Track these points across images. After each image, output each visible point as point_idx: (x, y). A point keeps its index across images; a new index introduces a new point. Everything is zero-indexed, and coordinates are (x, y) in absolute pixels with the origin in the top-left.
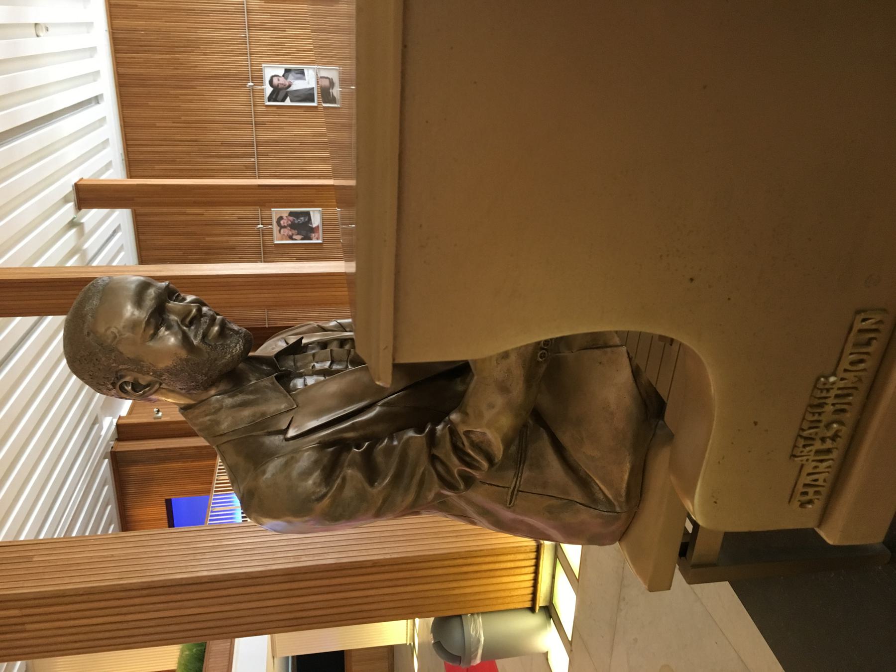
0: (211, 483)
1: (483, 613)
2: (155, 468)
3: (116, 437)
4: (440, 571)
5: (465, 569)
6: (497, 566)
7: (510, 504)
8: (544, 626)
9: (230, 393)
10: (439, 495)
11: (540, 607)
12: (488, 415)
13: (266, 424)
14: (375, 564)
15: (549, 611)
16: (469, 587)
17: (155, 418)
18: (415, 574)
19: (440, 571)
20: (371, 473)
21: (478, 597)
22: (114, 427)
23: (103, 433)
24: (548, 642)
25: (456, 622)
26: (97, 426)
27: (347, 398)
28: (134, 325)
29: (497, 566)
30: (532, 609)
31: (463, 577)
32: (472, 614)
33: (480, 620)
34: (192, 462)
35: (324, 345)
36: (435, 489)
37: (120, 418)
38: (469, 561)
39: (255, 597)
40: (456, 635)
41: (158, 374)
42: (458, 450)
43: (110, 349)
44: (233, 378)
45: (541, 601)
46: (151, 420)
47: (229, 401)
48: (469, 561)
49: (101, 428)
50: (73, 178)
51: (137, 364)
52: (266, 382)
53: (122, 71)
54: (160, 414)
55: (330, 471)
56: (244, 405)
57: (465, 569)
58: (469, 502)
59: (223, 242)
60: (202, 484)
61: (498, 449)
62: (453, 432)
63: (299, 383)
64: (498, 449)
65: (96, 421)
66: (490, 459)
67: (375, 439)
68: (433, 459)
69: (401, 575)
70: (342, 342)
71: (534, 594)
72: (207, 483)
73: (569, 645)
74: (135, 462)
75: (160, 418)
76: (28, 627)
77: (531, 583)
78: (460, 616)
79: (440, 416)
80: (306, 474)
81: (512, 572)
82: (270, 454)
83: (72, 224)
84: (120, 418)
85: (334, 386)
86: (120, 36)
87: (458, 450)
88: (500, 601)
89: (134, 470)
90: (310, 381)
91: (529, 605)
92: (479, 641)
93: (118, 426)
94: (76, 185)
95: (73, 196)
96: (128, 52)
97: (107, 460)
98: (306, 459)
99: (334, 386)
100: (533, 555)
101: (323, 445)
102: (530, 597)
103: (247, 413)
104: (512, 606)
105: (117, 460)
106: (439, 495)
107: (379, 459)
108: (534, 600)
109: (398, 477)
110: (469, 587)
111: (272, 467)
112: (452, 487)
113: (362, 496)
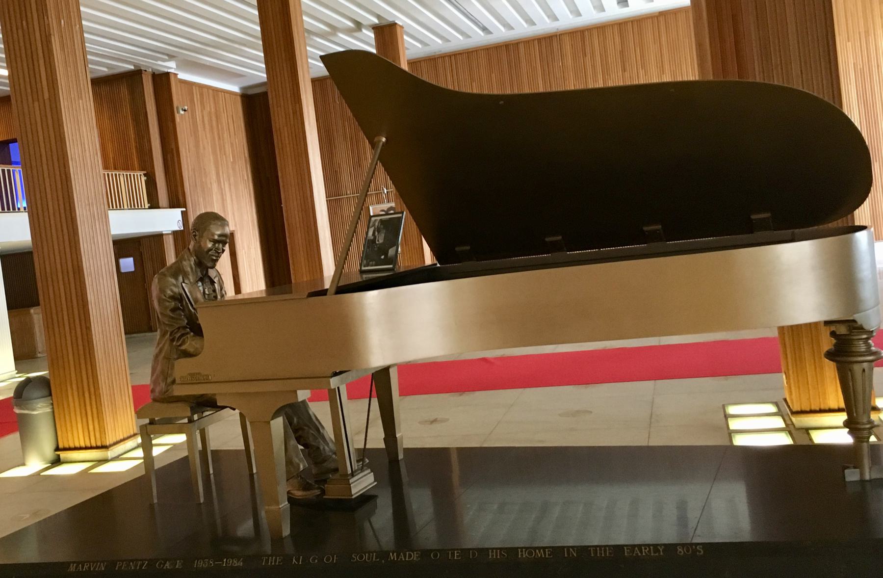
0: (115, 169)
1: (53, 412)
2: (127, 109)
3: (156, 73)
4: (84, 377)
5: (87, 395)
6: (90, 418)
7: (165, 358)
8: (44, 459)
9: (195, 264)
10: (167, 331)
11: (59, 456)
12: (193, 343)
13: (185, 275)
14: (88, 328)
15: (57, 462)
16: (73, 400)
17: (177, 108)
18: (82, 357)
19: (84, 377)
20: (173, 310)
21: (66, 406)
22: (166, 70)
23: (160, 63)
24: (34, 465)
25: (46, 392)
26: (166, 57)
27: (196, 301)
28: (213, 235)
29: (90, 418)
30: (57, 449)
31: (81, 393)
32: (52, 404)
33: (49, 410)
34: (136, 147)
35: (214, 291)
36: (169, 330)
37: (176, 75)
38: (93, 397)
39: (62, 248)
40: (37, 393)
41: (199, 242)
42: (183, 335)
43: (205, 229)
44: (200, 264)
45: (63, 455)
46: (176, 103)
47: (192, 263)
48: (93, 397)
49: (164, 60)
50: (401, 19)
51: (201, 237)
52: (199, 274)
53: (521, 47)
54: (182, 112)
55: (173, 298)
56: (191, 268)
57: (87, 395)
58: (164, 345)
59: (365, 153)
60: (114, 159)
61: (183, 347)
62: (187, 333)
63: (200, 284)
64: (183, 347)
65: (171, 57)
66: (180, 345)
67: (183, 311)
68: (179, 328)
69: (81, 347)
70: (216, 297)
71: (70, 449)
72: (114, 165)
73: (38, 474)
74: (132, 92)
75: (178, 112)
76: (36, 104)
77: (77, 445)
78: (51, 395)
79: (192, 330)
80: (172, 291)
81: (86, 430)
82: (177, 279)
83: (359, 25)
84: (176, 75)
85: (199, 296)
86: (555, 44)
87: (183, 335)
88: (63, 423)
89: (124, 91)
90: (201, 288)
91: (61, 446)
92: (34, 410)
93: (168, 73)
94: (396, 24)
95: (384, 23)
96: (540, 52)
97: (133, 67)
98: (176, 290)
99: (199, 296)
100: (99, 444)
101: (181, 295)
102: (67, 446)
103: (189, 269)
104: (59, 433)
105: (134, 77)
106: (167, 331)
107: (178, 312)
108: (65, 449)
109: (172, 318)
110: (73, 400)
111: (173, 281)
112: (171, 335)
113: (166, 308)
